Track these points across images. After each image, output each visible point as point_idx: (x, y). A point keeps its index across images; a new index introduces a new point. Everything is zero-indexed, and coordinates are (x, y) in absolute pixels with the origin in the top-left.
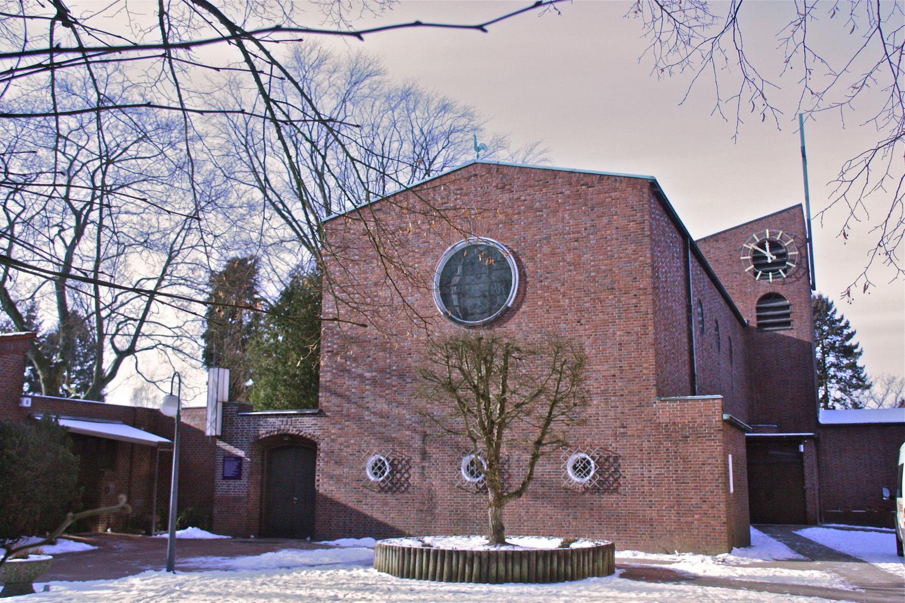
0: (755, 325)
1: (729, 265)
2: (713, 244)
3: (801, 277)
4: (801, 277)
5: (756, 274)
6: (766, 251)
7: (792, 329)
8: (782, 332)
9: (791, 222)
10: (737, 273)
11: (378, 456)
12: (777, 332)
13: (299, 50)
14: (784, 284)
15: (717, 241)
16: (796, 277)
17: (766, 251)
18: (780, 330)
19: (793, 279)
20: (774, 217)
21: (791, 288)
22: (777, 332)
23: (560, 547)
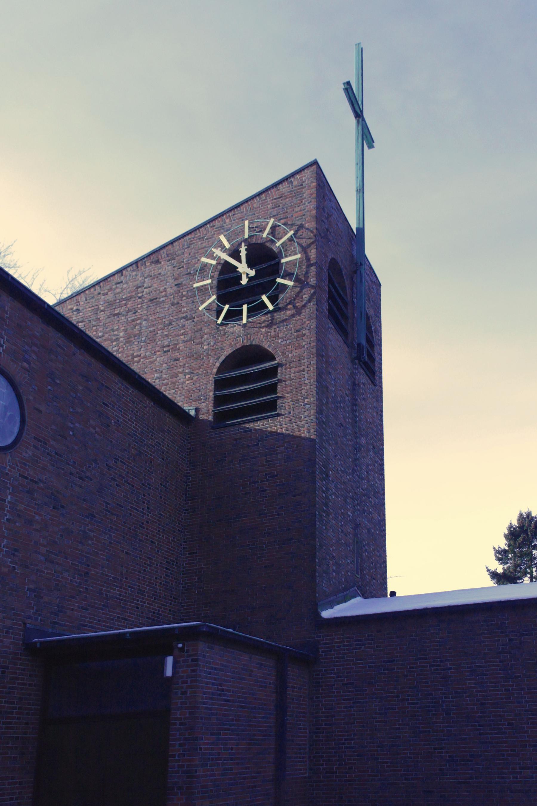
0: (207, 415)
1: (173, 304)
2: (149, 268)
3: (304, 306)
4: (304, 306)
5: (219, 312)
6: (240, 261)
7: (278, 415)
8: (259, 425)
9: (295, 201)
10: (185, 318)
11: (33, 594)
12: (250, 425)
13: (120, 316)
14: (271, 325)
15: (158, 262)
16: (295, 307)
17: (240, 261)
18: (257, 420)
19: (289, 313)
20: (263, 196)
21: (283, 331)
22: (250, 425)
23: (360, 596)
